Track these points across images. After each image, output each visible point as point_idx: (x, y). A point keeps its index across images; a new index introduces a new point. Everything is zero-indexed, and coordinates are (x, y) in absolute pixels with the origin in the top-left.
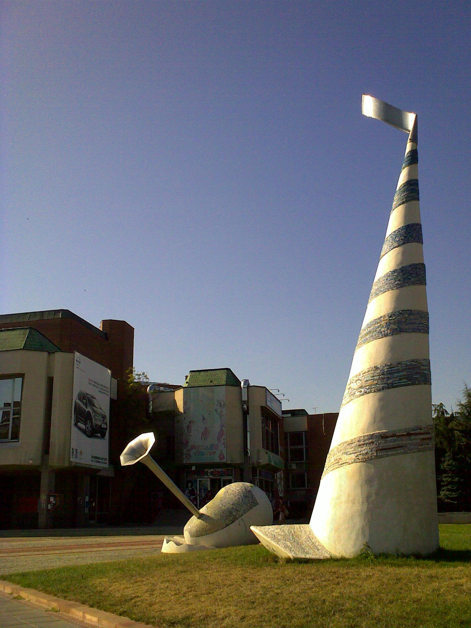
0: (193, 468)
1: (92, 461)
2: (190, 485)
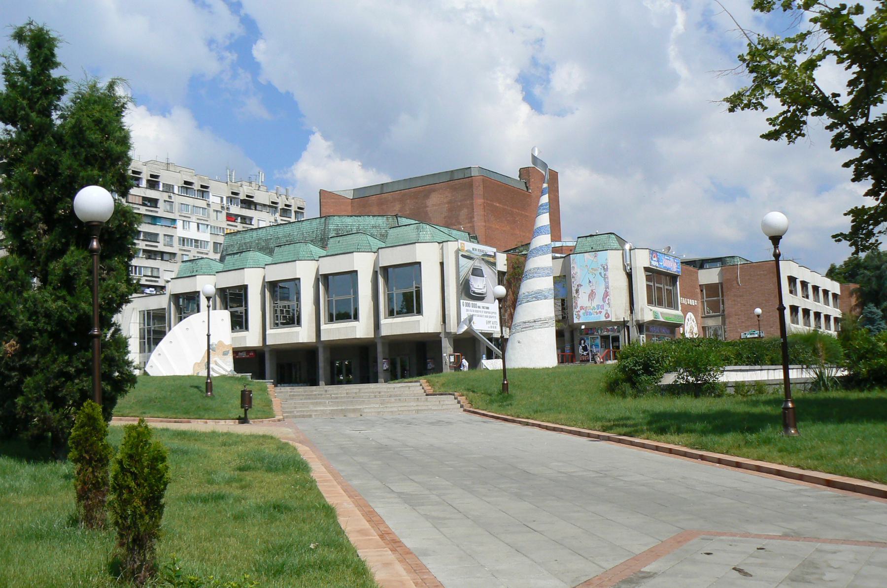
2: (583, 342)
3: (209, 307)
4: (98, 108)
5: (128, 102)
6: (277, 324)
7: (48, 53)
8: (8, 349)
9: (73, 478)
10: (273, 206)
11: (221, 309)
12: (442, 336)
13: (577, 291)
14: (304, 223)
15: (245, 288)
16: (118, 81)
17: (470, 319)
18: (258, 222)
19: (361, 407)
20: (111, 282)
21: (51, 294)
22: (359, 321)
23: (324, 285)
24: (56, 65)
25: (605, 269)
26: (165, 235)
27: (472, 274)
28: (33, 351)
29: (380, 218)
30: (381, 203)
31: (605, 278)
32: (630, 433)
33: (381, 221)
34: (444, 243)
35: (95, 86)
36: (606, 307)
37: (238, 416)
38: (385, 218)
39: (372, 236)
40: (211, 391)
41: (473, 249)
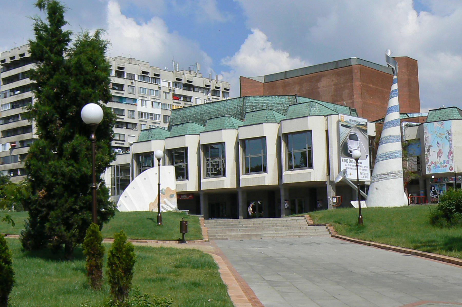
0: (432, 176)
1: (144, 106)
2: (433, 188)
3: (159, 165)
4: (89, 49)
5: (108, 44)
6: (209, 174)
7: (60, 17)
8: (41, 195)
9: (79, 270)
10: (206, 88)
11: (168, 165)
12: (327, 183)
13: (429, 150)
14: (228, 102)
15: (186, 149)
16: (101, 31)
17: (345, 172)
18: (196, 101)
19: (262, 233)
20: (100, 155)
21: (65, 163)
22: (267, 173)
23: (242, 147)
24: (64, 23)
25: (450, 134)
26: (129, 110)
27: (350, 139)
28: (53, 197)
29: (283, 97)
30: (285, 86)
31: (450, 140)
32: (430, 250)
33: (284, 99)
34: (329, 116)
35: (88, 35)
36: (450, 162)
37: (178, 239)
38: (287, 98)
39: (277, 110)
40: (161, 222)
41: (350, 120)
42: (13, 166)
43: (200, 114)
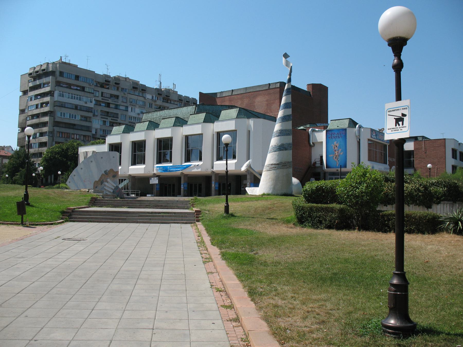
42: (35, 151)
43: (164, 116)
